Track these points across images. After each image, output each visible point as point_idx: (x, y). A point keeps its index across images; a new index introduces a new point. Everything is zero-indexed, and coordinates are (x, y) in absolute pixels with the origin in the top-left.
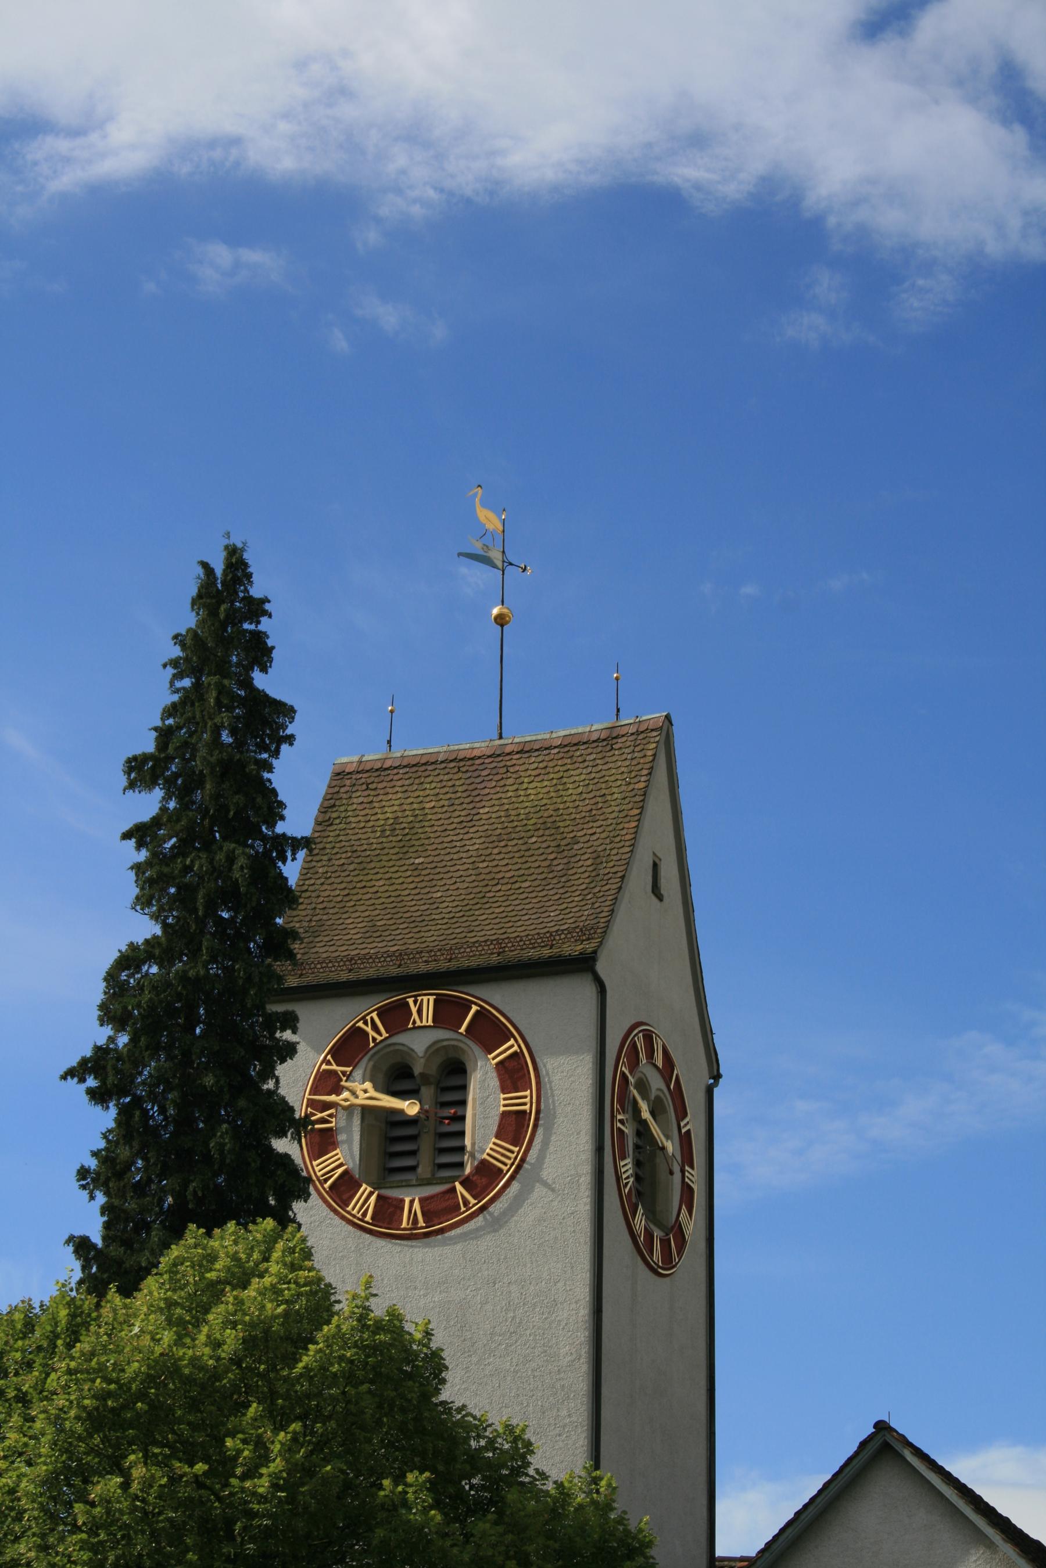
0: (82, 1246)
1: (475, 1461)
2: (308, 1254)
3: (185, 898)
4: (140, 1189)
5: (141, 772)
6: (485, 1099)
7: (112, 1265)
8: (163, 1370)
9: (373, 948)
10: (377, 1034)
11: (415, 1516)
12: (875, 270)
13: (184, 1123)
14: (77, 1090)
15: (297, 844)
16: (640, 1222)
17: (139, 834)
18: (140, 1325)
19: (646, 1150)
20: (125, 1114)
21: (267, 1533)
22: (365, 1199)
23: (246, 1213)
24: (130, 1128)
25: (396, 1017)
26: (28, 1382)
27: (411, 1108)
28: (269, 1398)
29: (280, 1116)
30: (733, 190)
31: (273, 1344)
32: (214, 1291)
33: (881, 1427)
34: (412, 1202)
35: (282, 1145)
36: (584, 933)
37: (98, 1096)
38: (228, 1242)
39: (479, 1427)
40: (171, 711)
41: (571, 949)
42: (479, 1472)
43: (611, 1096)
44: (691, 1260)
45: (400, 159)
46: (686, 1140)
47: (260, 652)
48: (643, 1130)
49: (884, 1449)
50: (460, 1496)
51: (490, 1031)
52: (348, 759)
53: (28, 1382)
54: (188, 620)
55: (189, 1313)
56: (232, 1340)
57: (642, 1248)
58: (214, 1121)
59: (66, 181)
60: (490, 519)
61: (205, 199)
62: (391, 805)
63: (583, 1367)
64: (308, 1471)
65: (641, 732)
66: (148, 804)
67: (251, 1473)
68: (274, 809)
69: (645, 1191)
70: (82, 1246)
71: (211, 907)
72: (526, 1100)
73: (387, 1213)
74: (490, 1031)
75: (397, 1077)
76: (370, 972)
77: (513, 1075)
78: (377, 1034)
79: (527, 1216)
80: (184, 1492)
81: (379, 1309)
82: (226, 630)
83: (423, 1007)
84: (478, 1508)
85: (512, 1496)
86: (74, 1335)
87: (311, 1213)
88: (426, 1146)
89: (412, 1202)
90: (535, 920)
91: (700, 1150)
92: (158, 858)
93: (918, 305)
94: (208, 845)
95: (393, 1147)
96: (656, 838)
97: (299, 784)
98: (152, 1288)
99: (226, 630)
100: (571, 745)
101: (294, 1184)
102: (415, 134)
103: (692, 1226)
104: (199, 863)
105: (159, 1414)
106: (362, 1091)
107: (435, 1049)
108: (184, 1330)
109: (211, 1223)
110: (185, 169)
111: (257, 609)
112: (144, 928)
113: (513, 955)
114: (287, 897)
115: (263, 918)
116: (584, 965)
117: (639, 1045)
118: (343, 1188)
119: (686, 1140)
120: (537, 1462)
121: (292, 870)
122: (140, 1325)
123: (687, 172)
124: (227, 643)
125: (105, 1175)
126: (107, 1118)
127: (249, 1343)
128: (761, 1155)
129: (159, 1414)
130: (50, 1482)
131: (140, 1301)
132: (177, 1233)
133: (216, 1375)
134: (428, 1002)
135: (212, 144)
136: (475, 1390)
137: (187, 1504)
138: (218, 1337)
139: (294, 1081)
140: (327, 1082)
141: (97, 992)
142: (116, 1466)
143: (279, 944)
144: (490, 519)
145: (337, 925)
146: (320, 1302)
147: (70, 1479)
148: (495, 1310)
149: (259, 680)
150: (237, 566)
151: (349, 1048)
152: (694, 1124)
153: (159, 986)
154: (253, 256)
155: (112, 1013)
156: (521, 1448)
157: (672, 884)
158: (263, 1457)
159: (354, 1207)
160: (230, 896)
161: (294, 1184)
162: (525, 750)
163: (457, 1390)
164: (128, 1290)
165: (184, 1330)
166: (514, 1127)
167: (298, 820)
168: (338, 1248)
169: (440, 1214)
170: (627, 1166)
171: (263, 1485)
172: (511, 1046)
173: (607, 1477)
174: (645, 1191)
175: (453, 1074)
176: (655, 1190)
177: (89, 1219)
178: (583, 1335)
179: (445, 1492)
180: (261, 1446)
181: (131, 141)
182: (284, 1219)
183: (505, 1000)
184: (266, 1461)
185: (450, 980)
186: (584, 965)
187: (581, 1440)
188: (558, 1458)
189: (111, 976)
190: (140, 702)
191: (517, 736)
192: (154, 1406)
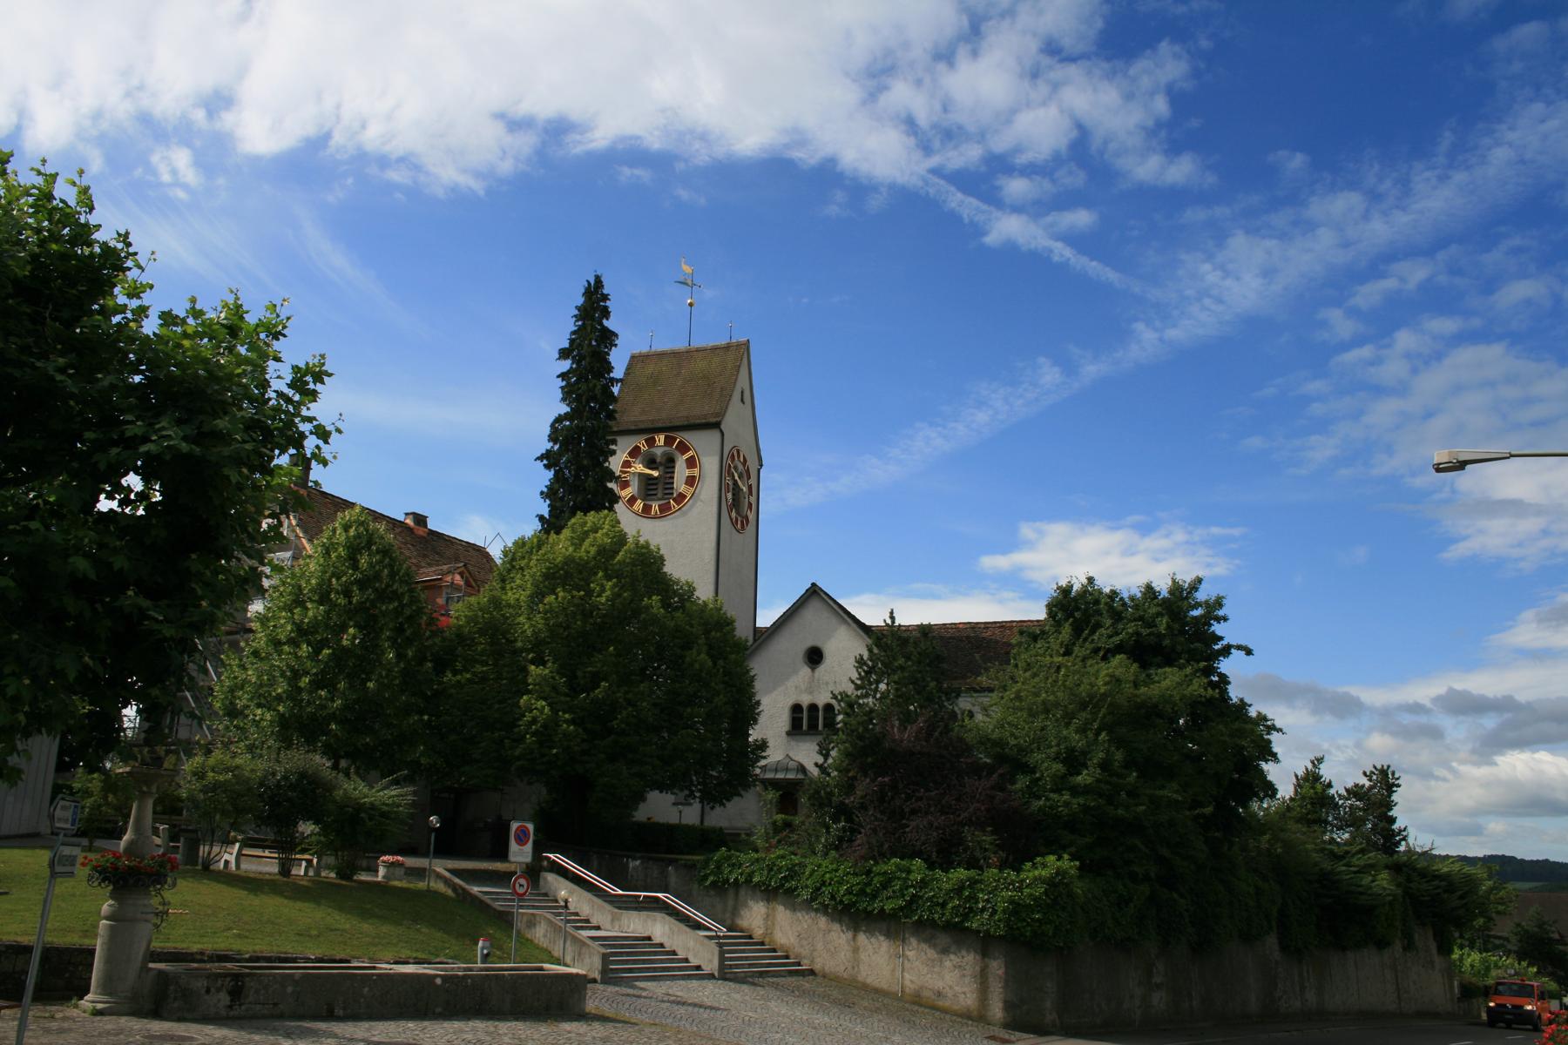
0: (541, 518)
1: (675, 592)
2: (618, 522)
3: (578, 399)
4: (562, 499)
5: (564, 354)
6: (681, 471)
7: (552, 524)
8: (569, 561)
9: (644, 418)
10: (644, 448)
11: (655, 610)
12: (859, 188)
13: (577, 477)
14: (540, 465)
15: (618, 381)
16: (734, 514)
17: (563, 376)
18: (562, 544)
19: (736, 490)
20: (556, 473)
21: (605, 616)
22: (639, 505)
23: (599, 507)
24: (558, 477)
25: (651, 442)
26: (523, 563)
27: (655, 474)
28: (606, 570)
29: (611, 475)
30: (813, 162)
31: (606, 553)
32: (586, 534)
33: (814, 585)
34: (655, 506)
35: (610, 485)
36: (717, 415)
37: (547, 467)
38: (592, 517)
39: (677, 583)
40: (573, 333)
41: (713, 420)
42: (675, 596)
43: (725, 471)
44: (750, 528)
45: (697, 145)
46: (750, 487)
47: (606, 313)
48: (735, 483)
49: (814, 592)
50: (669, 605)
51: (683, 448)
52: (636, 351)
53: (523, 563)
54: (580, 301)
55: (578, 542)
56: (593, 550)
57: (734, 523)
58: (587, 476)
59: (578, 150)
60: (687, 269)
61: (629, 154)
62: (650, 369)
63: (713, 563)
64: (619, 595)
65: (739, 345)
66: (566, 365)
67: (599, 595)
68: (610, 369)
69: (736, 504)
70: (541, 518)
71: (588, 402)
72: (696, 472)
73: (647, 509)
74: (683, 448)
75: (651, 463)
76: (642, 426)
77: (691, 463)
78: (644, 448)
79: (222, 946)
80: (576, 601)
81: (642, 540)
82: (594, 304)
83: (660, 439)
84: (677, 609)
85: (688, 605)
86: (539, 547)
87: (619, 507)
88: (660, 487)
89: (655, 506)
90: (701, 409)
91: (754, 490)
92: (568, 384)
93: (875, 203)
94: (587, 380)
95: (649, 487)
96: (742, 382)
97: (619, 361)
98: (566, 533)
99: (594, 304)
100: (714, 349)
101: (615, 499)
102: (704, 137)
103: (751, 516)
104: (583, 387)
105: (568, 575)
106: (639, 468)
107: (664, 454)
108: (578, 546)
109: (586, 512)
110: (621, 147)
111: (605, 298)
112: (564, 409)
113: (692, 422)
114: (613, 399)
115: (604, 406)
116: (716, 425)
117: (735, 454)
118: (632, 501)
119: (750, 487)
120: (696, 594)
121: (616, 390)
122: (562, 544)
123: (797, 154)
124: (595, 310)
125: (550, 494)
126: (550, 474)
127: (599, 553)
128: (776, 497)
129: (568, 575)
130: (531, 596)
131: (562, 537)
132: (573, 514)
133: (587, 562)
134: (662, 437)
135: (631, 138)
136: (674, 568)
137: (577, 606)
138: (588, 549)
139: (615, 463)
140: (627, 464)
141: (548, 430)
142: (553, 592)
143: (611, 415)
144: (687, 269)
145: (630, 413)
146: (621, 539)
147: (538, 595)
148: (684, 544)
149: (605, 322)
150: (598, 281)
151: (635, 452)
152: (753, 481)
153: (568, 429)
154: (637, 172)
155: (553, 438)
156: (692, 590)
157: (748, 399)
158: (603, 590)
159: (635, 507)
160: (594, 398)
161: (615, 499)
162: (698, 350)
163: (668, 568)
164: (558, 533)
165: (578, 546)
166: (691, 481)
167: (618, 373)
168: (630, 521)
169: (665, 509)
170: (730, 496)
171: (603, 600)
172: (691, 453)
173: (720, 598)
174: (736, 504)
175: (670, 462)
176: (739, 503)
177: (544, 509)
178: (713, 553)
179: (666, 604)
180: (602, 586)
181: (601, 136)
182: (611, 509)
183: (690, 437)
184: (605, 592)
185: (670, 429)
186: (716, 425)
187: (711, 588)
188: (704, 593)
189: (552, 426)
190: (562, 328)
191: (697, 343)
192: (566, 572)
